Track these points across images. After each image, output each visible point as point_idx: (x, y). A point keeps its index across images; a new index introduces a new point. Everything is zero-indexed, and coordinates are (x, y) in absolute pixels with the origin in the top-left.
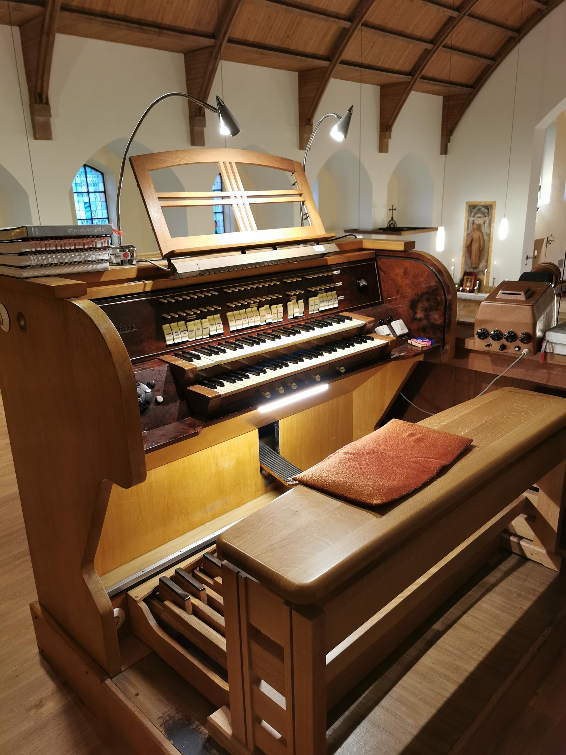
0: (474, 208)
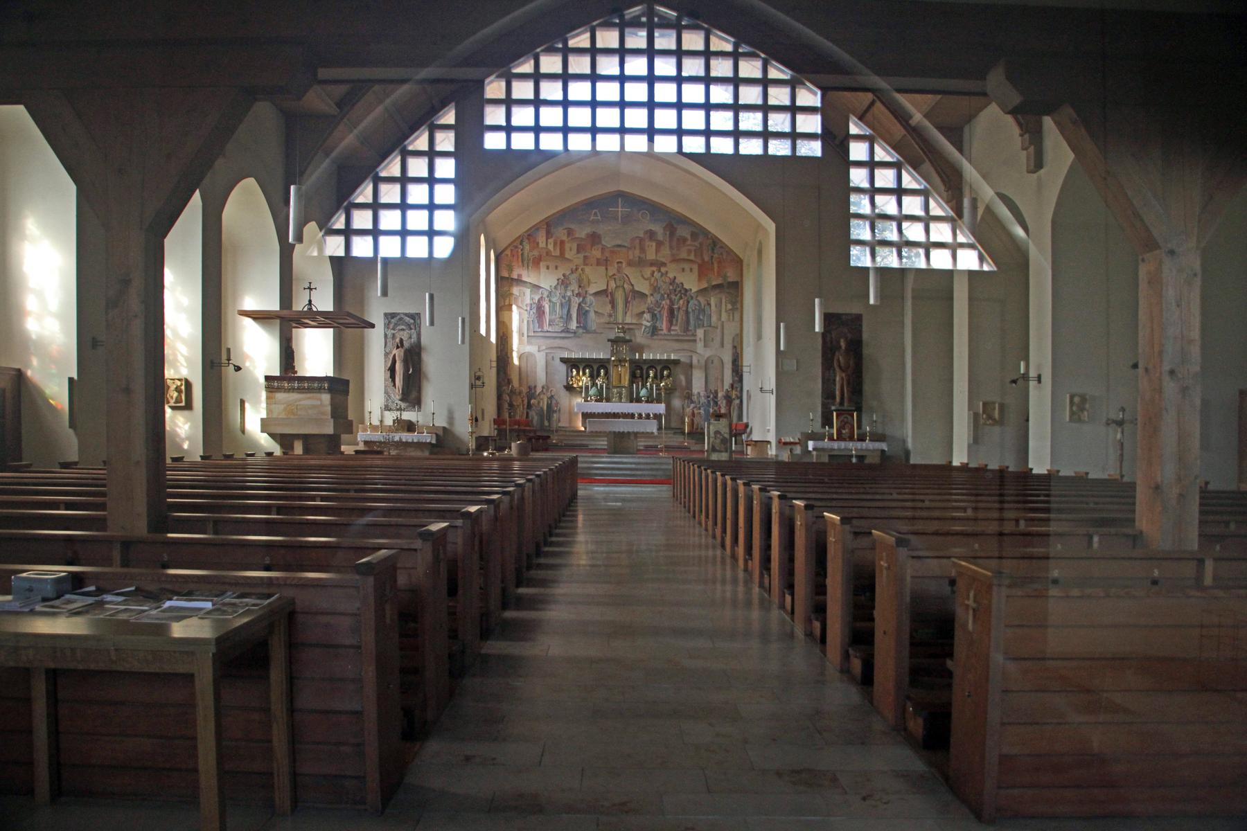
0: (393, 318)
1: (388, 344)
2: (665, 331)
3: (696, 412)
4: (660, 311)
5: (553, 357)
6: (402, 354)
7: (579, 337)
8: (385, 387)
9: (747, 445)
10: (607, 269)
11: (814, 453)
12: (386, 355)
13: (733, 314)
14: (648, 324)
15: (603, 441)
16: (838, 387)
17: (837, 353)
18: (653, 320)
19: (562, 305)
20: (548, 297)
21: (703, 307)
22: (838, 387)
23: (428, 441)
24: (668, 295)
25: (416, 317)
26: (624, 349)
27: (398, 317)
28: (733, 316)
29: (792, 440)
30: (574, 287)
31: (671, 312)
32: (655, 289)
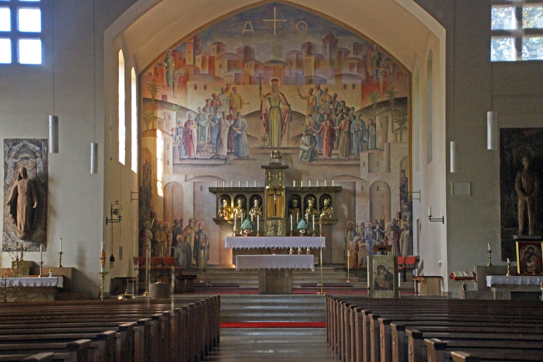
0: (15, 144)
1: (9, 175)
2: (325, 156)
3: (360, 245)
4: (320, 133)
5: (201, 187)
6: (25, 185)
7: (230, 164)
8: (4, 224)
9: (417, 281)
10: (260, 88)
11: (494, 290)
12: (6, 187)
13: (401, 134)
14: (306, 148)
15: (255, 279)
16: (520, 213)
17: (518, 174)
18: (311, 143)
19: (211, 129)
20: (196, 120)
21: (367, 127)
22: (520, 213)
23: (53, 285)
24: (328, 116)
25: (41, 143)
26: (279, 176)
27: (21, 144)
28: (401, 137)
29: (466, 275)
30: (225, 108)
31: (332, 134)
32: (315, 109)
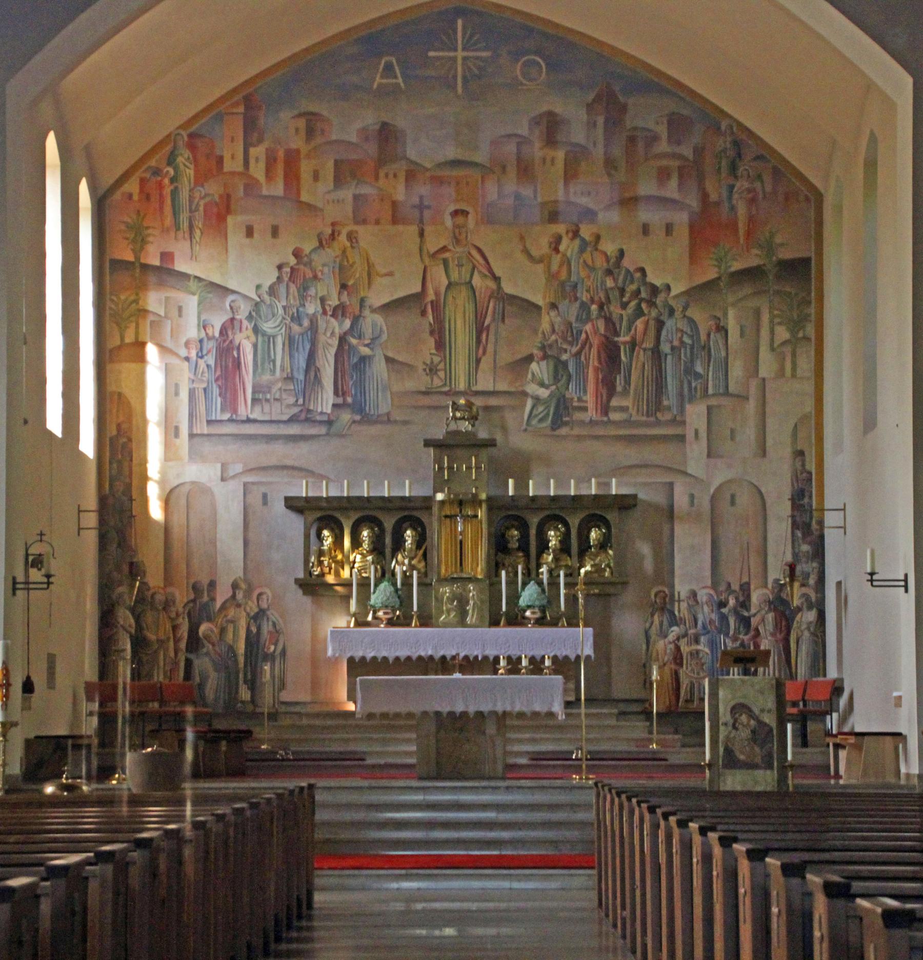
2: (592, 413)
3: (685, 649)
4: (578, 353)
5: (265, 496)
7: (342, 436)
9: (837, 746)
10: (422, 234)
13: (794, 355)
14: (544, 393)
15: (408, 741)
18: (556, 378)
19: (291, 343)
20: (250, 317)
21: (703, 337)
24: (601, 307)
30: (328, 288)
